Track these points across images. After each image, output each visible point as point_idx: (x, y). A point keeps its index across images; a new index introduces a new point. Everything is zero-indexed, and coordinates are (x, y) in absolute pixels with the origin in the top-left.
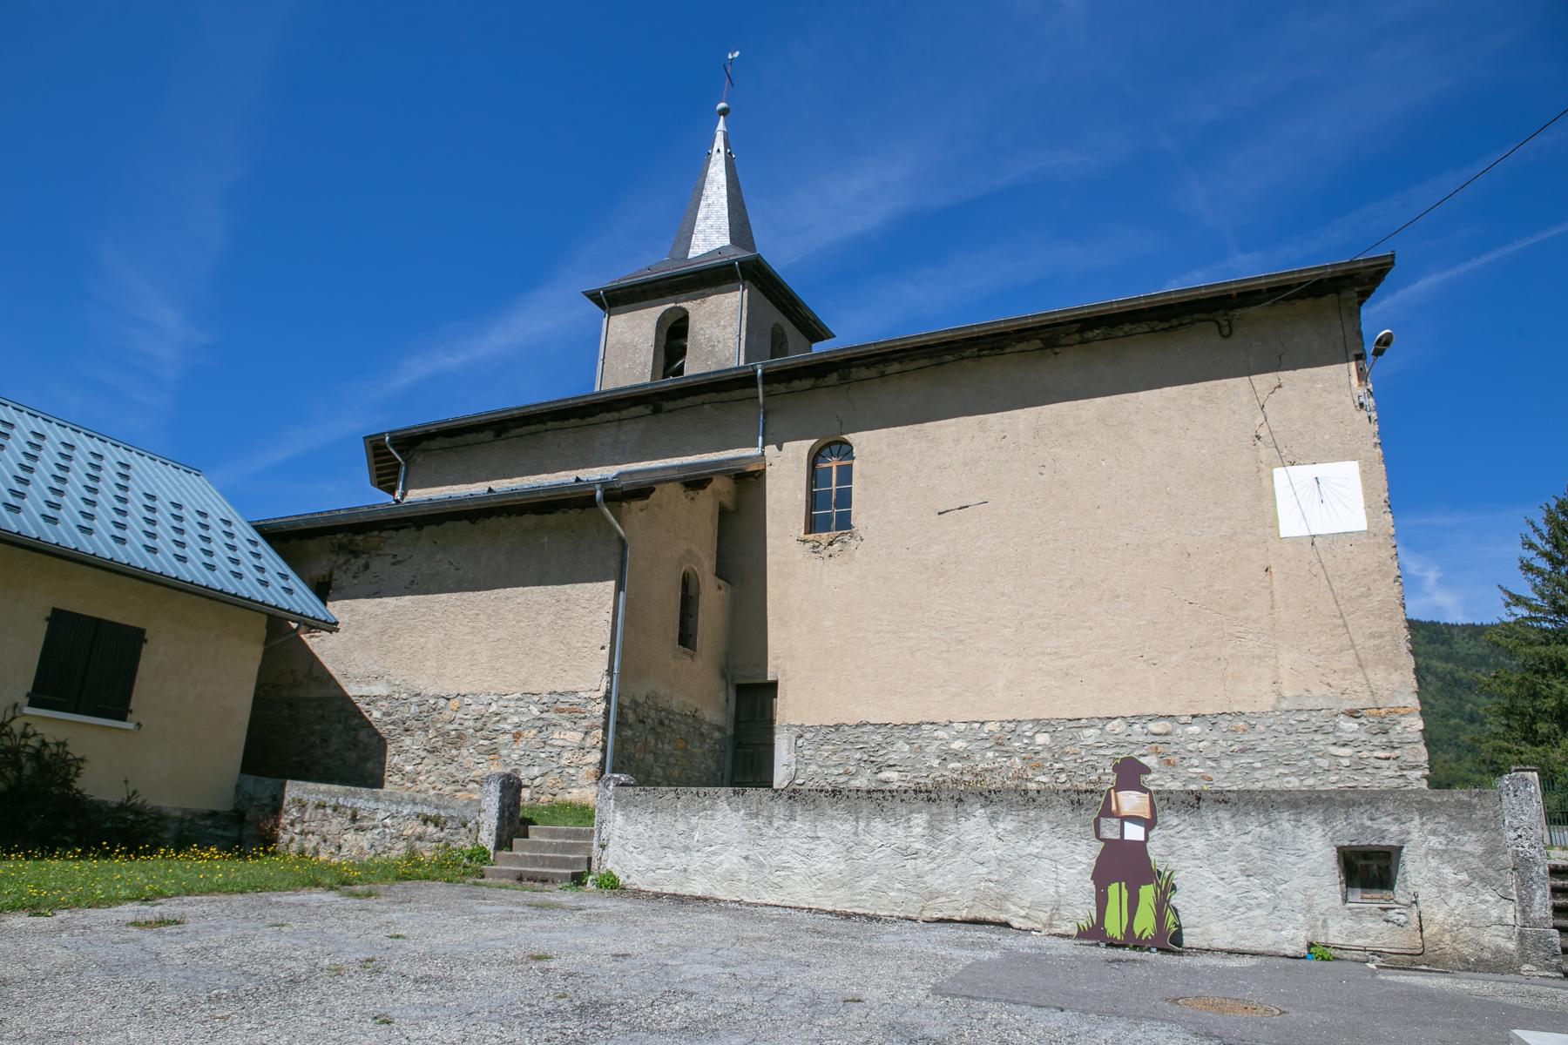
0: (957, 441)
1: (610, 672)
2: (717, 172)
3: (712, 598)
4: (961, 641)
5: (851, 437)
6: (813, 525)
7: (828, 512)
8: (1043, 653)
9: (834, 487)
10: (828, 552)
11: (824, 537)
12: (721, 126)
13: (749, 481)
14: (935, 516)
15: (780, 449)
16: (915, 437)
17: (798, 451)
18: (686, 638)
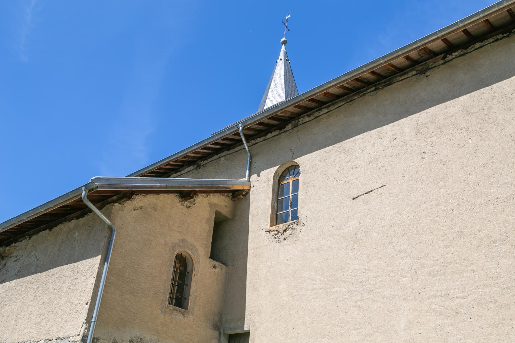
0: (363, 149)
1: (88, 320)
2: (280, 70)
3: (205, 275)
4: (370, 292)
5: (298, 161)
6: (276, 220)
7: (284, 211)
8: (435, 296)
9: (291, 195)
10: (283, 237)
11: (281, 227)
12: (283, 48)
13: (239, 196)
14: (350, 202)
15: (259, 176)
16: (337, 152)
17: (269, 174)
18: (179, 298)
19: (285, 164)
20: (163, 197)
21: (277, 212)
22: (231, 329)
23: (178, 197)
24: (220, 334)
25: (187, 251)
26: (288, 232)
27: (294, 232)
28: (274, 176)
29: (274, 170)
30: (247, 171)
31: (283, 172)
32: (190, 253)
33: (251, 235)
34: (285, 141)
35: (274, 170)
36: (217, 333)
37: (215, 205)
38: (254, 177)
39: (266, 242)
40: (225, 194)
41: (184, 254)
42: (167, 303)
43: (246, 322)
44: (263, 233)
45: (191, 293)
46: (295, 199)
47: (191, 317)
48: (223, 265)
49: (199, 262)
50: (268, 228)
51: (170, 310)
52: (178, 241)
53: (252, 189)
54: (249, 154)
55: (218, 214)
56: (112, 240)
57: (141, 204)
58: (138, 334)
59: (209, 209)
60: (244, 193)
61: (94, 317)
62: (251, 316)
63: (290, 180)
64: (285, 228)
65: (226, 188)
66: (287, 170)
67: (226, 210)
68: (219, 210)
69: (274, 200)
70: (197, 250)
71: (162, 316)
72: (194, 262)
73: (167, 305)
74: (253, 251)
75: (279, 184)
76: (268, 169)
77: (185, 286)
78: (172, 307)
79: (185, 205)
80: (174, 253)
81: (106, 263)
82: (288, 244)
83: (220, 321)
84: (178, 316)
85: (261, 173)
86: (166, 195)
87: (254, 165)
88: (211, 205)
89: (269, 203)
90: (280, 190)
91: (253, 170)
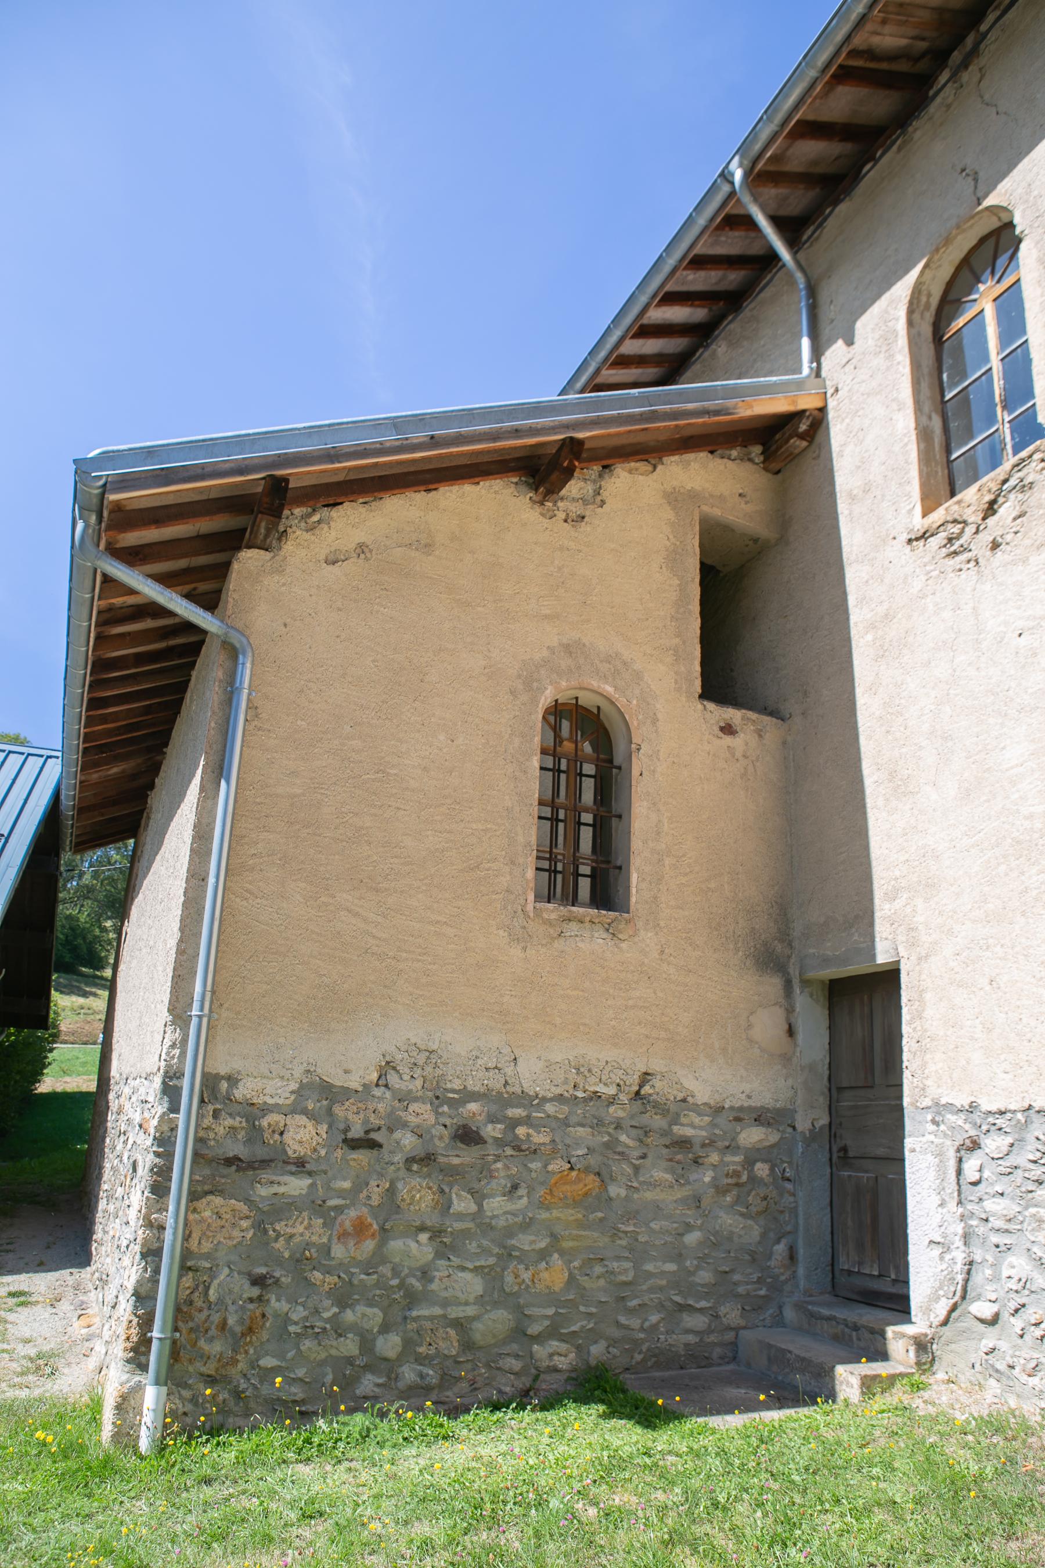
3: (687, 768)
10: (986, 537)
11: (972, 496)
13: (787, 442)
15: (850, 342)
19: (948, 241)
20: (453, 497)
21: (948, 451)
22: (826, 961)
23: (523, 488)
24: (788, 985)
25: (597, 687)
26: (1006, 510)
27: (1032, 502)
28: (910, 312)
29: (902, 290)
30: (805, 343)
31: (950, 285)
32: (609, 689)
33: (855, 577)
34: (933, 147)
35: (902, 290)
36: (773, 985)
37: (693, 496)
38: (836, 353)
39: (917, 584)
40: (734, 453)
41: (587, 700)
42: (531, 897)
43: (881, 929)
44: (899, 553)
45: (636, 844)
46: (1019, 365)
47: (648, 937)
48: (766, 719)
49: (655, 721)
50: (919, 523)
51: (549, 923)
52: (545, 653)
53: (831, 404)
54: (799, 277)
55: (713, 535)
56: (240, 689)
57: (360, 536)
58: (416, 1036)
59: (669, 514)
60: (803, 427)
61: (197, 997)
62: (898, 904)
63: (984, 301)
64: (989, 497)
65: (717, 413)
66: (966, 273)
67: (749, 508)
68: (716, 512)
69: (927, 407)
70: (638, 676)
71: (516, 952)
72: (633, 724)
73: (530, 907)
74: (869, 637)
75: (938, 338)
76: (878, 296)
77: (614, 820)
78: (553, 911)
79: (562, 515)
80: (534, 701)
81: (223, 783)
82: (1014, 563)
83: (785, 935)
84: (585, 939)
85: (859, 325)
86: (468, 489)
87: (828, 312)
88: (674, 498)
89: (905, 422)
90: (947, 362)
91: (826, 331)
